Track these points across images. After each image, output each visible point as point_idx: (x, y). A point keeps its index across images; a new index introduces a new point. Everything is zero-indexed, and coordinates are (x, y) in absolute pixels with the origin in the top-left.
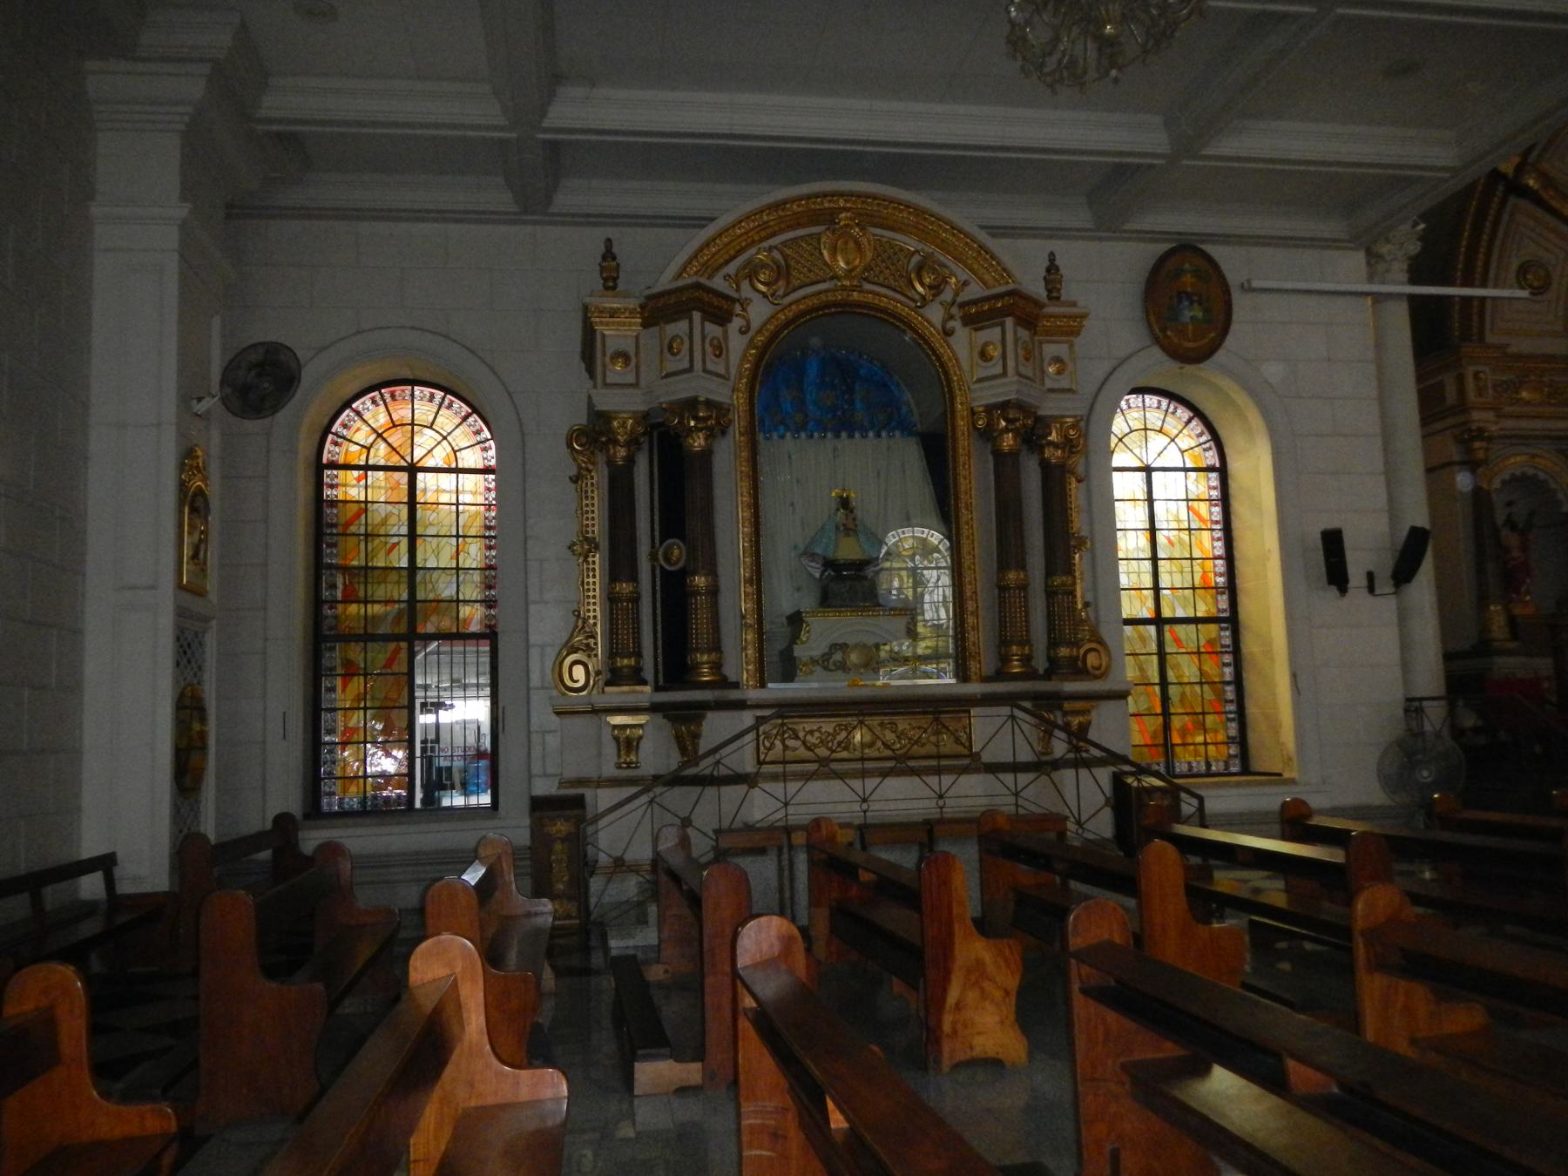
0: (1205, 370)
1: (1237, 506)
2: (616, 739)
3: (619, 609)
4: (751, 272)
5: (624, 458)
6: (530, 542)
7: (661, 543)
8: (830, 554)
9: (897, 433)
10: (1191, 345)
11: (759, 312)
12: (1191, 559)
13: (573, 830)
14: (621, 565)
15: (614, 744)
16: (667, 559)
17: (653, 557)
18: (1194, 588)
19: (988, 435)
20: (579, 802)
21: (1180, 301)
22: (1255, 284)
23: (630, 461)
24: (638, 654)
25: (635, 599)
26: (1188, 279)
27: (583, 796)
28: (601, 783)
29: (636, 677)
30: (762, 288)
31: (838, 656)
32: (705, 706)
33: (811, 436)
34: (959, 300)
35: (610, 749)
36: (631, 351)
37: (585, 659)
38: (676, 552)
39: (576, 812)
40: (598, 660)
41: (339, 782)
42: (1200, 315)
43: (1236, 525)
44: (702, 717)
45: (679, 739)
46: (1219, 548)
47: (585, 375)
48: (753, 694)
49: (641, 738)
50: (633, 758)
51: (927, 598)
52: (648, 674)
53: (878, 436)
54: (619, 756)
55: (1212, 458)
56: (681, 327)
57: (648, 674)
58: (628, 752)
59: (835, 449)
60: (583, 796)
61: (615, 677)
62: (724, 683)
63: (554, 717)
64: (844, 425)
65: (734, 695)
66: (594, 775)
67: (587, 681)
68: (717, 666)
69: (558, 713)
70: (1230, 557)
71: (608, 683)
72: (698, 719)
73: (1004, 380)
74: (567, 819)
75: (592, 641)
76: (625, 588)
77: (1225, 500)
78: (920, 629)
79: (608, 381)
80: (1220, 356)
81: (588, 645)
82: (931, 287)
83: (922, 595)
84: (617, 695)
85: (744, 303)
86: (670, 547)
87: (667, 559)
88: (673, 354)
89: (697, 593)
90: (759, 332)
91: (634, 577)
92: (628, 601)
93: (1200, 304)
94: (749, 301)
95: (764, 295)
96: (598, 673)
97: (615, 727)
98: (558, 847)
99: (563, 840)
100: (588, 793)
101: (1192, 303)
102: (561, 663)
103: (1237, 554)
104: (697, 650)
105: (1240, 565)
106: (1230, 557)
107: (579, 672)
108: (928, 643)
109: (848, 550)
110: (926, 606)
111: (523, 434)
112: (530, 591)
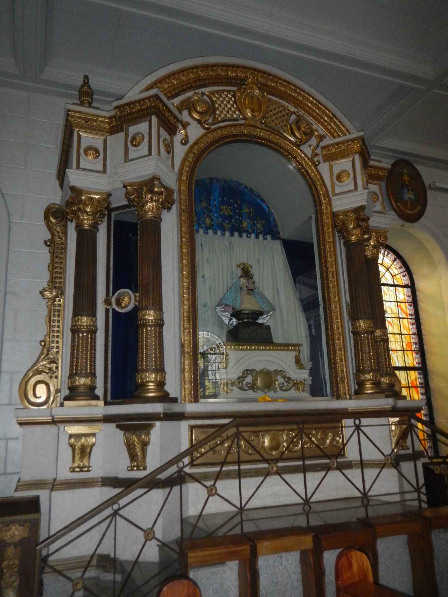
0: (414, 229)
1: (422, 305)
2: (72, 446)
3: (81, 340)
4: (189, 106)
5: (89, 225)
6: (8, 296)
7: (114, 293)
8: (238, 306)
9: (269, 237)
10: (410, 212)
11: (195, 132)
12: (401, 334)
13: (26, 534)
14: (84, 302)
15: (70, 449)
16: (118, 303)
17: (107, 302)
18: (404, 350)
19: (343, 231)
20: (33, 505)
21: (403, 189)
22: (438, 185)
23: (95, 226)
24: (93, 375)
25: (93, 332)
26: (406, 178)
27: (38, 497)
28: (55, 485)
29: (90, 394)
30: (196, 116)
31: (249, 379)
32: (155, 417)
33: (216, 233)
34: (322, 144)
35: (66, 454)
36: (101, 148)
37: (47, 380)
38: (126, 299)
39: (31, 516)
40: (61, 381)
41: (406, 301)
42: (413, 197)
43: (422, 315)
44: (151, 426)
45: (130, 447)
46: (413, 329)
47: (59, 188)
48: (191, 408)
49: (94, 445)
50: (86, 462)
51: (210, 368)
52: (99, 391)
53: (257, 237)
54: (74, 461)
55: (405, 281)
56: (143, 127)
57: (99, 391)
58: (82, 458)
59: (231, 243)
60: (38, 497)
61: (73, 394)
62: (164, 398)
63: (18, 426)
64: (237, 229)
65: (176, 408)
66: (49, 476)
67: (48, 397)
68: (161, 384)
69: (21, 424)
70: (419, 334)
71: (67, 398)
72: (147, 428)
73: (356, 193)
74: (22, 523)
75: (54, 365)
76: (85, 321)
77: (414, 302)
78: (207, 384)
79: (81, 166)
80: (422, 220)
81: (50, 369)
82: (305, 134)
83: (207, 366)
84: (75, 408)
85: (185, 126)
86: (123, 294)
87: (118, 303)
88: (135, 146)
89: (145, 325)
90: (196, 143)
91: (93, 314)
92: (88, 332)
93: (412, 190)
94: (188, 124)
95: (199, 122)
96: (57, 391)
97: (71, 436)
98: (10, 551)
99: (15, 545)
100: (43, 494)
101: (409, 190)
102: (27, 383)
103: (423, 332)
104: (146, 370)
105: (425, 338)
106: (419, 334)
107: (41, 390)
108: (210, 390)
109: (248, 304)
110: (210, 373)
111: (10, 222)
112: (6, 331)
